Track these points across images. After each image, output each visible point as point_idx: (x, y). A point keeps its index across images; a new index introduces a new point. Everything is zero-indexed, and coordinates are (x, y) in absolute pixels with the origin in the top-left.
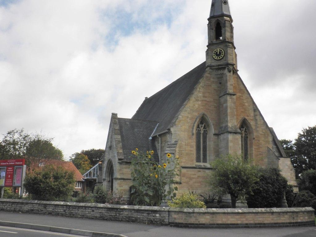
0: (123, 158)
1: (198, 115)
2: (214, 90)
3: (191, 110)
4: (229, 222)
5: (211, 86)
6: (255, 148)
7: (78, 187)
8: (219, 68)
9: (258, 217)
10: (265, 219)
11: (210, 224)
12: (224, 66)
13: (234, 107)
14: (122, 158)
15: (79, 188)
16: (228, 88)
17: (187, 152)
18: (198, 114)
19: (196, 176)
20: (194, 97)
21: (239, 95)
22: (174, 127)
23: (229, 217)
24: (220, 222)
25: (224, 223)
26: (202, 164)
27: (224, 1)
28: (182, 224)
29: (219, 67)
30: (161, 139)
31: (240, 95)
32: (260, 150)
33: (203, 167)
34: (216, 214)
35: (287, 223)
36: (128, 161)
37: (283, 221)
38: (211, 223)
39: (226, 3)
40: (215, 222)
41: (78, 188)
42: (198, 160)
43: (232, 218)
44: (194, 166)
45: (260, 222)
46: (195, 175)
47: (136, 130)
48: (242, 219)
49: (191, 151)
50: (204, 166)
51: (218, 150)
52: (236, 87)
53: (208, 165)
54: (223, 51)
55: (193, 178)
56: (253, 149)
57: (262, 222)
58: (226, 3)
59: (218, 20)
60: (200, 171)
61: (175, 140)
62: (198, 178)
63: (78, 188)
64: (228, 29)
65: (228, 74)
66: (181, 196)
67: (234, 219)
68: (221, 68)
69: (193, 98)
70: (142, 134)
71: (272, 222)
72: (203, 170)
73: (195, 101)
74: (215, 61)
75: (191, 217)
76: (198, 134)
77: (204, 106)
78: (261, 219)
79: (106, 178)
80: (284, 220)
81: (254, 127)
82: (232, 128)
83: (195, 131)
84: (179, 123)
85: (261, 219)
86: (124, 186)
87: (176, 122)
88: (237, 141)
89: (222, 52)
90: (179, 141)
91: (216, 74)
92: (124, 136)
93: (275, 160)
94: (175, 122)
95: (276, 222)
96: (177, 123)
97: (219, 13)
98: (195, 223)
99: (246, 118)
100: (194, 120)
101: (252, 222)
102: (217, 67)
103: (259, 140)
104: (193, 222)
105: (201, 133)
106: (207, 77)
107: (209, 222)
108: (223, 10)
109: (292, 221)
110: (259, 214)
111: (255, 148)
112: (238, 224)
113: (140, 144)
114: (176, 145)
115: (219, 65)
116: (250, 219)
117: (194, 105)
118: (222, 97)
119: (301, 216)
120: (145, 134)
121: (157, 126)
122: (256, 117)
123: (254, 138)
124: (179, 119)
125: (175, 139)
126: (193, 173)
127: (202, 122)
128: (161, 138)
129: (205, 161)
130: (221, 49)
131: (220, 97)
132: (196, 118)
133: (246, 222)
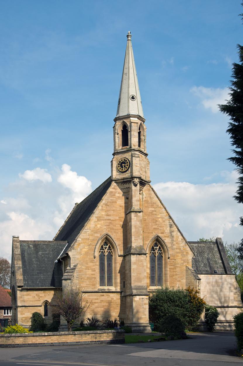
0: (23, 285)
1: (100, 237)
2: (120, 206)
3: (92, 231)
4: (37, 342)
5: (116, 202)
6: (170, 269)
7: (8, 314)
8: (124, 181)
9: (62, 338)
10: (68, 339)
11: (23, 344)
12: (129, 180)
13: (140, 226)
14: (22, 285)
15: (9, 315)
16: (133, 204)
17: (88, 276)
18: (101, 235)
19: (99, 301)
20: (96, 217)
21: (151, 210)
22: (73, 251)
23: (37, 339)
24: (30, 343)
25: (34, 343)
26: (106, 288)
27: (131, 97)
28: (4, 345)
29: (125, 180)
30: (64, 263)
31: (153, 209)
32: (176, 270)
33: (107, 291)
34: (27, 337)
35: (89, 342)
36: (29, 288)
37: (84, 341)
38: (23, 343)
39: (134, 98)
40: (27, 343)
41: (8, 315)
42: (102, 283)
43: (39, 339)
44: (96, 290)
45: (63, 342)
46: (98, 299)
47: (40, 253)
48: (48, 340)
49: (94, 274)
50: (108, 289)
51: (125, 272)
52: (148, 201)
53: (113, 289)
54: (128, 161)
55: (95, 303)
56: (168, 269)
57: (65, 342)
58: (134, 98)
59: (124, 121)
60: (103, 295)
61: (74, 264)
62: (101, 302)
63: (8, 315)
64: (135, 133)
65: (133, 188)
66: (9, 326)
67: (41, 340)
68: (127, 181)
69: (95, 217)
70: (48, 257)
71: (75, 341)
72: (107, 294)
73: (97, 222)
74: (119, 174)
75: (9, 340)
76: (102, 257)
77: (108, 226)
78: (64, 339)
79: (13, 306)
80: (86, 339)
81: (169, 245)
82: (135, 249)
83: (97, 254)
84: (78, 246)
85: (64, 339)
86: (25, 314)
87: (75, 246)
88: (142, 263)
89: (127, 163)
90: (79, 265)
91: (122, 188)
92: (27, 261)
93: (193, 280)
94: (74, 245)
95: (77, 341)
96: (75, 246)
97: (125, 114)
98: (12, 344)
99: (160, 235)
100: (96, 242)
101: (56, 342)
102: (122, 181)
103: (175, 259)
104: (10, 344)
105: (105, 255)
106: (111, 192)
107: (22, 343)
108: (130, 109)
109: (94, 340)
110: (62, 336)
111: (170, 269)
112: (44, 344)
113: (44, 268)
114: (74, 270)
115: (124, 179)
116: (55, 340)
117: (96, 225)
118: (128, 214)
119: (105, 336)
120: (50, 257)
121: (66, 246)
122: (172, 233)
123: (169, 258)
124: (78, 241)
125: (73, 263)
126: (96, 297)
127: (106, 244)
128: (64, 261)
129: (110, 283)
130: (126, 159)
131: (127, 214)
132: (98, 239)
133: (52, 342)
